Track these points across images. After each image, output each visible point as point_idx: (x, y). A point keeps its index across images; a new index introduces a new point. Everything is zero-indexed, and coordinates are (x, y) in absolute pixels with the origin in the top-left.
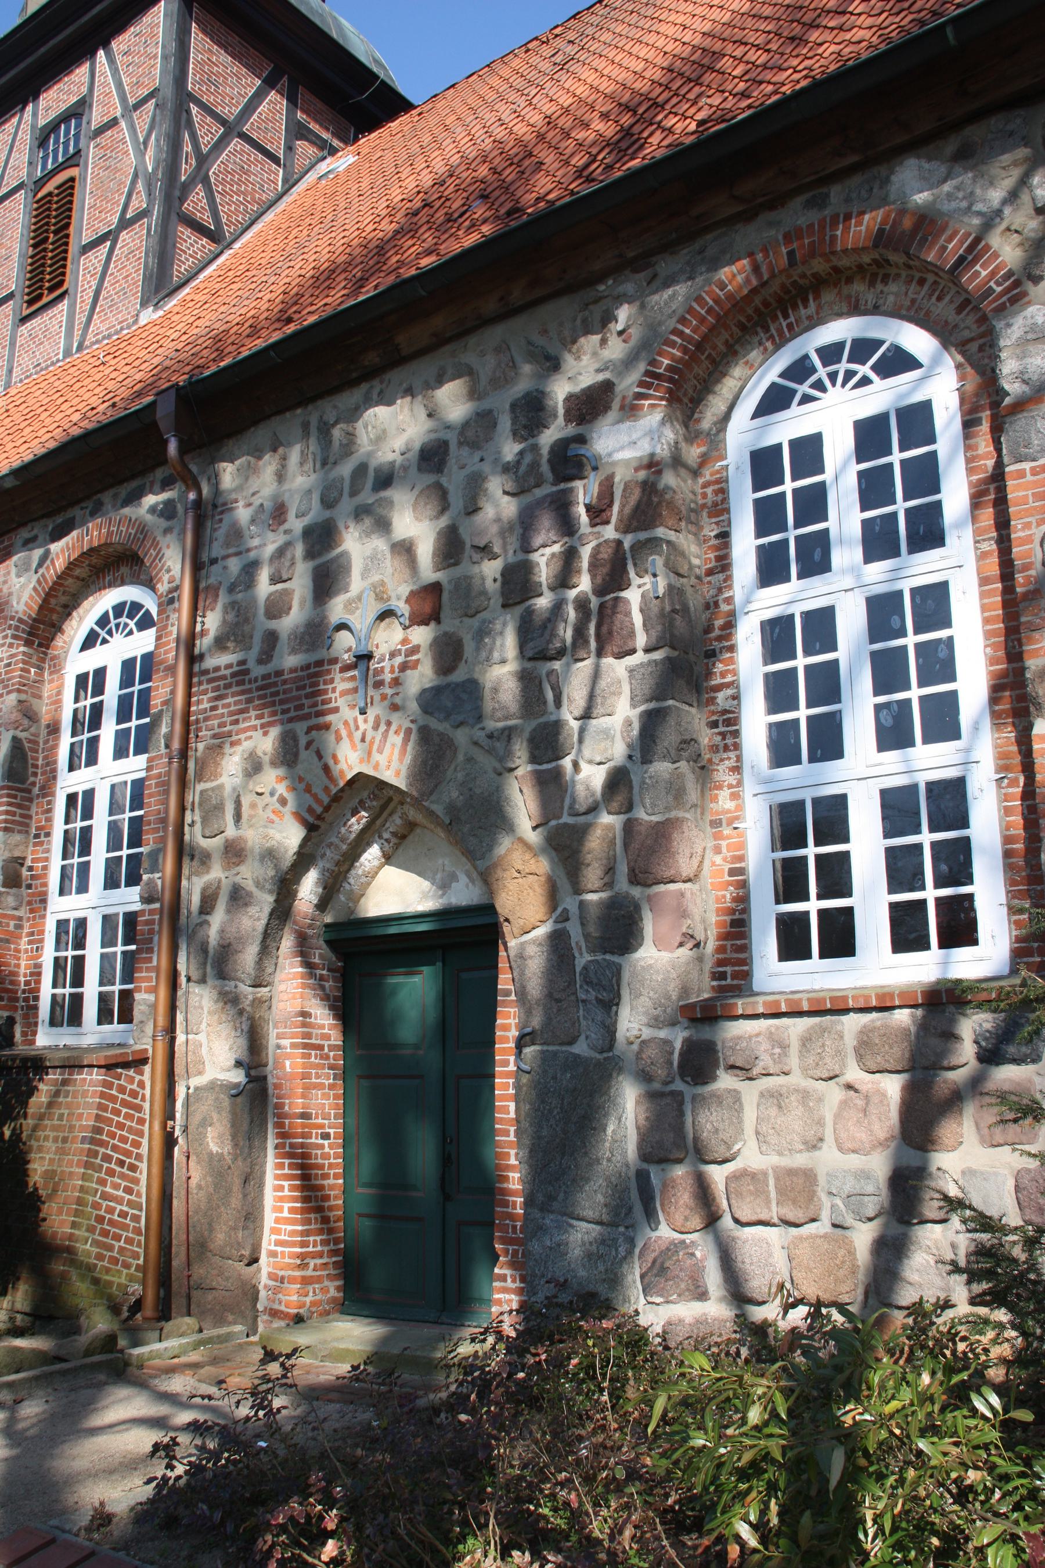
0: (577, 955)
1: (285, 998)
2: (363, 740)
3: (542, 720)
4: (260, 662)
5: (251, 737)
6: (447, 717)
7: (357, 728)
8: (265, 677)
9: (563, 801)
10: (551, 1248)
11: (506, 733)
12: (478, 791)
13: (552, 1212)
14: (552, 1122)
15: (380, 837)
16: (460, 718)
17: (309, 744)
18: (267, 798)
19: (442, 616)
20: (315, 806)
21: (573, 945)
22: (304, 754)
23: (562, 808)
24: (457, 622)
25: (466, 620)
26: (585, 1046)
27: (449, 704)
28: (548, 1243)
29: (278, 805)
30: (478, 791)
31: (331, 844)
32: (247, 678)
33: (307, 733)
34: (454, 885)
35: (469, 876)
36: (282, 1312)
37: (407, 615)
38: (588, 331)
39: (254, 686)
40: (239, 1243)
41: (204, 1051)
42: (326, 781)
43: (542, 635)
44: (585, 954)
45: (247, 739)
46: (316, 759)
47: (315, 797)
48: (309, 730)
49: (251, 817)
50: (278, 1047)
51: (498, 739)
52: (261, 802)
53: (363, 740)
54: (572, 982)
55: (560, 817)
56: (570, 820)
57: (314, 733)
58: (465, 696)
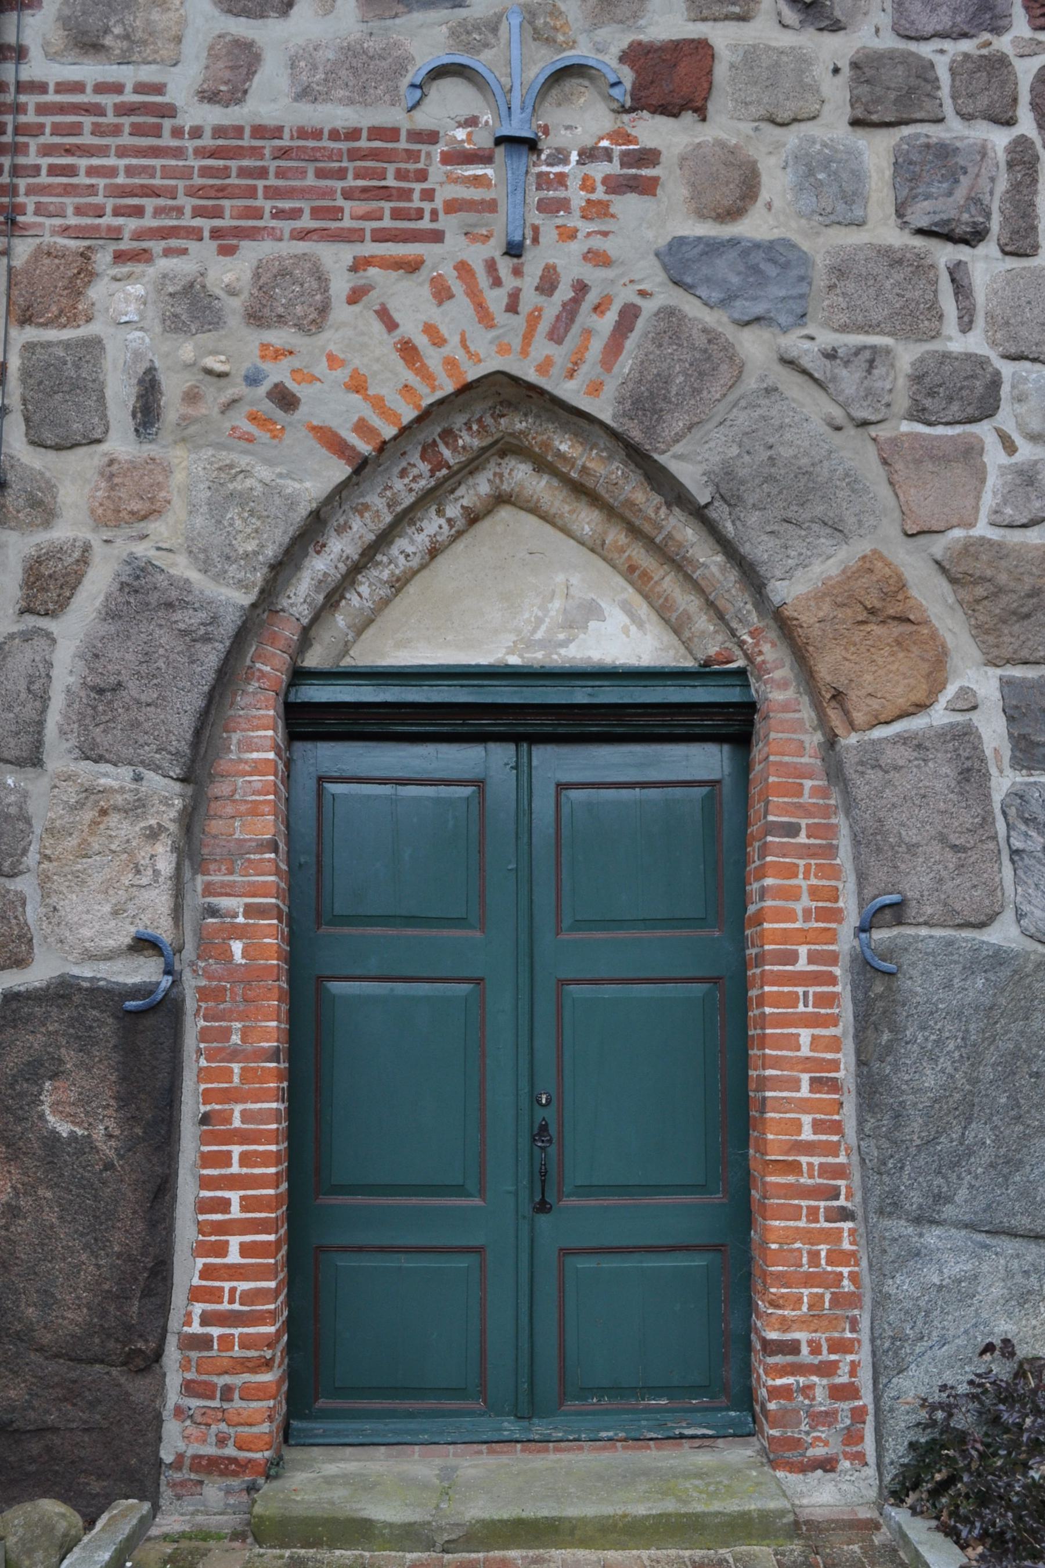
0: (993, 771)
1: (229, 810)
2: (512, 307)
3: (935, 346)
4: (209, 97)
5: (184, 252)
6: (725, 303)
7: (497, 282)
8: (219, 132)
9: (978, 498)
10: (940, 1288)
11: (867, 354)
12: (786, 452)
13: (938, 1223)
14: (944, 1062)
15: (440, 512)
16: (759, 309)
17: (355, 297)
18: (237, 388)
19: (711, 107)
20: (376, 421)
21: (989, 753)
22: (341, 312)
23: (976, 509)
24: (747, 127)
25: (767, 128)
26: (1014, 931)
27: (735, 280)
28: (936, 1280)
29: (268, 407)
30: (786, 452)
31: (366, 507)
32: (167, 124)
33: (354, 268)
34: (592, 624)
35: (627, 609)
36: (234, 1460)
37: (628, 85)
38: (12, 9)
39: (190, 145)
40: (129, 1328)
41: (32, 913)
42: (409, 377)
43: (950, 194)
44: (1008, 771)
45: (168, 253)
46: (377, 327)
47: (378, 404)
48: (358, 265)
49: (185, 421)
50: (213, 911)
51: (847, 363)
52: (215, 396)
53: (512, 307)
54: (987, 820)
55: (972, 525)
56: (994, 534)
57: (372, 271)
58: (771, 271)
